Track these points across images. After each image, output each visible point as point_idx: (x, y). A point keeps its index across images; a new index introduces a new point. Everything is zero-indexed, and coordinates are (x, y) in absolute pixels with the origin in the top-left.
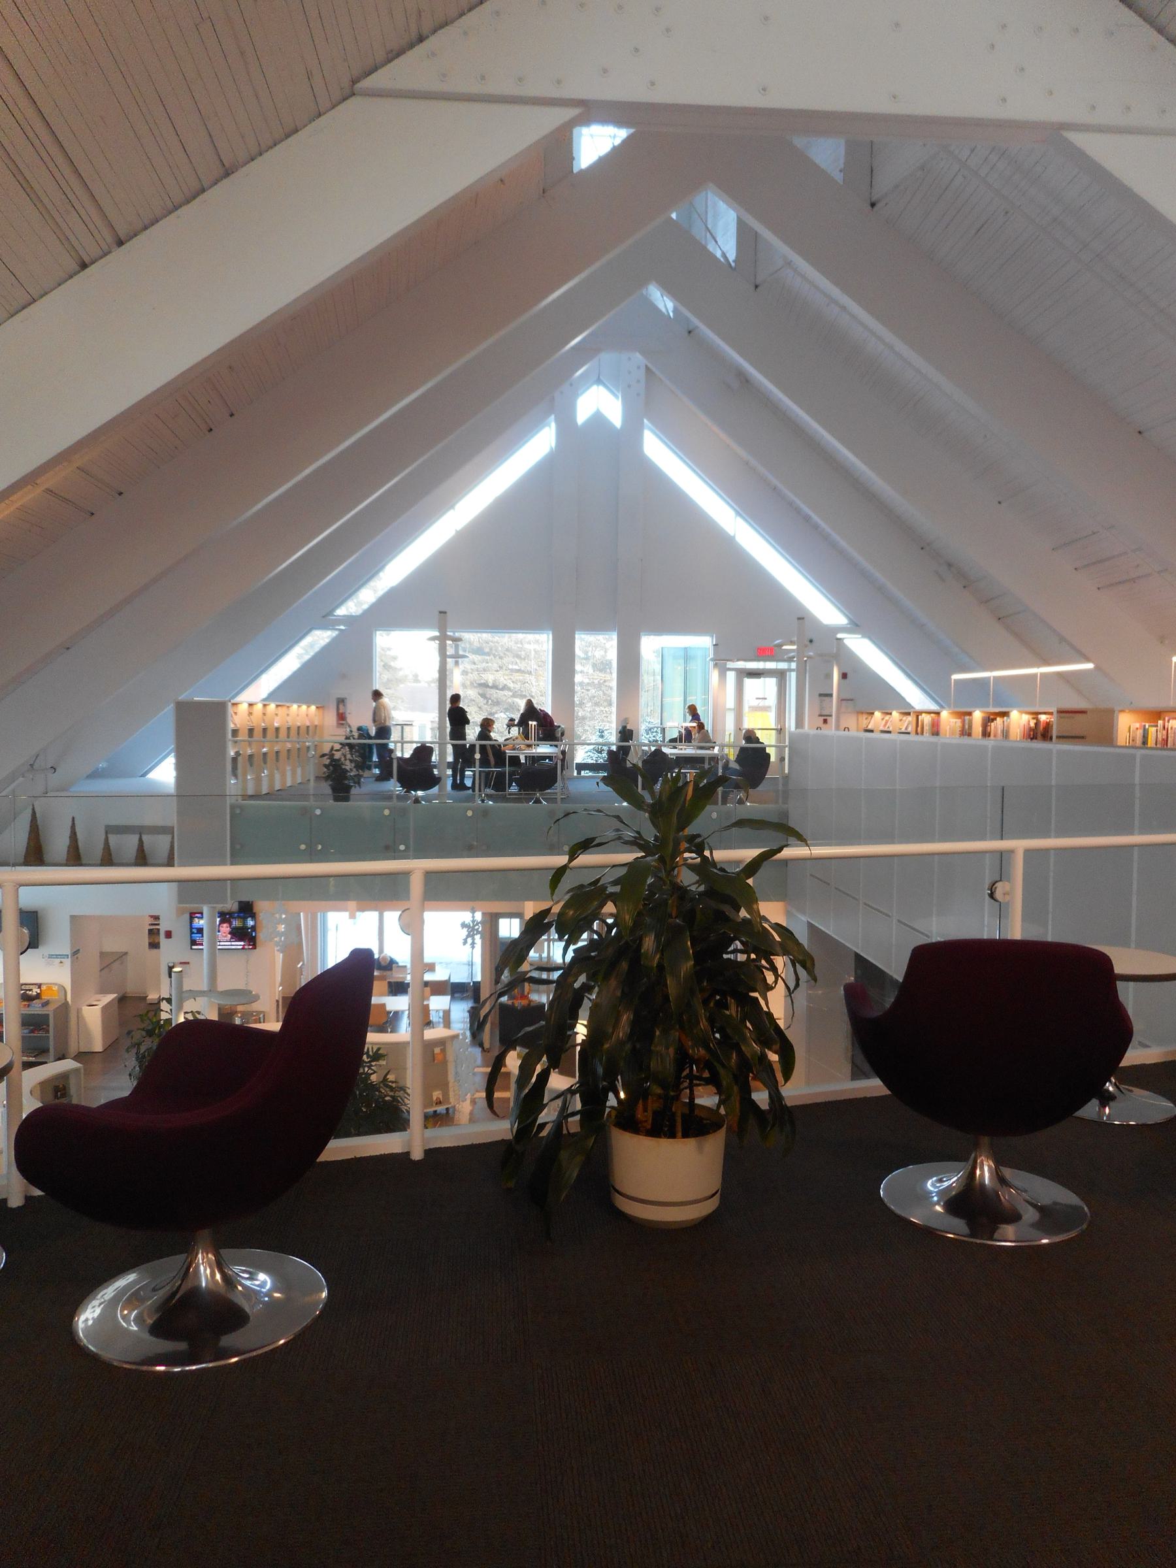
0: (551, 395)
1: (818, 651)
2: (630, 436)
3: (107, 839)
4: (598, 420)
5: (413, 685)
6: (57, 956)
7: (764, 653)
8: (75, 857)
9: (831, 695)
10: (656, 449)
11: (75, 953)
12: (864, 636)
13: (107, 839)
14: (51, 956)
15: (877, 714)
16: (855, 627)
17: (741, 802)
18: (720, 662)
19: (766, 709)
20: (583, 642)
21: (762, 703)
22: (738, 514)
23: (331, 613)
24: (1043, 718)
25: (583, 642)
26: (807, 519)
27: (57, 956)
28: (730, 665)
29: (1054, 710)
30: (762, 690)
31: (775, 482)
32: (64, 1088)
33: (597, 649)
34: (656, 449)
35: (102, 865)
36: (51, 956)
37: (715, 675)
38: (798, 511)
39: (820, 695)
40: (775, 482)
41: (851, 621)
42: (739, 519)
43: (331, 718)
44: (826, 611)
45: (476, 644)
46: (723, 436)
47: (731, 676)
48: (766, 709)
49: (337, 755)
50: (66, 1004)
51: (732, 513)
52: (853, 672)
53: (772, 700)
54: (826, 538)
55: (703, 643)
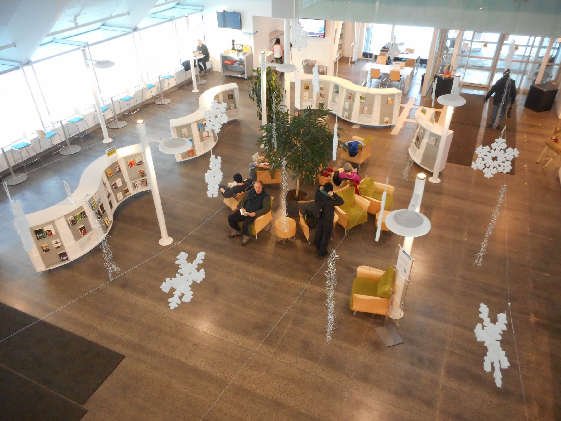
6: (249, 34)
11: (256, 32)
14: (246, 33)
27: (249, 34)
32: (232, 95)
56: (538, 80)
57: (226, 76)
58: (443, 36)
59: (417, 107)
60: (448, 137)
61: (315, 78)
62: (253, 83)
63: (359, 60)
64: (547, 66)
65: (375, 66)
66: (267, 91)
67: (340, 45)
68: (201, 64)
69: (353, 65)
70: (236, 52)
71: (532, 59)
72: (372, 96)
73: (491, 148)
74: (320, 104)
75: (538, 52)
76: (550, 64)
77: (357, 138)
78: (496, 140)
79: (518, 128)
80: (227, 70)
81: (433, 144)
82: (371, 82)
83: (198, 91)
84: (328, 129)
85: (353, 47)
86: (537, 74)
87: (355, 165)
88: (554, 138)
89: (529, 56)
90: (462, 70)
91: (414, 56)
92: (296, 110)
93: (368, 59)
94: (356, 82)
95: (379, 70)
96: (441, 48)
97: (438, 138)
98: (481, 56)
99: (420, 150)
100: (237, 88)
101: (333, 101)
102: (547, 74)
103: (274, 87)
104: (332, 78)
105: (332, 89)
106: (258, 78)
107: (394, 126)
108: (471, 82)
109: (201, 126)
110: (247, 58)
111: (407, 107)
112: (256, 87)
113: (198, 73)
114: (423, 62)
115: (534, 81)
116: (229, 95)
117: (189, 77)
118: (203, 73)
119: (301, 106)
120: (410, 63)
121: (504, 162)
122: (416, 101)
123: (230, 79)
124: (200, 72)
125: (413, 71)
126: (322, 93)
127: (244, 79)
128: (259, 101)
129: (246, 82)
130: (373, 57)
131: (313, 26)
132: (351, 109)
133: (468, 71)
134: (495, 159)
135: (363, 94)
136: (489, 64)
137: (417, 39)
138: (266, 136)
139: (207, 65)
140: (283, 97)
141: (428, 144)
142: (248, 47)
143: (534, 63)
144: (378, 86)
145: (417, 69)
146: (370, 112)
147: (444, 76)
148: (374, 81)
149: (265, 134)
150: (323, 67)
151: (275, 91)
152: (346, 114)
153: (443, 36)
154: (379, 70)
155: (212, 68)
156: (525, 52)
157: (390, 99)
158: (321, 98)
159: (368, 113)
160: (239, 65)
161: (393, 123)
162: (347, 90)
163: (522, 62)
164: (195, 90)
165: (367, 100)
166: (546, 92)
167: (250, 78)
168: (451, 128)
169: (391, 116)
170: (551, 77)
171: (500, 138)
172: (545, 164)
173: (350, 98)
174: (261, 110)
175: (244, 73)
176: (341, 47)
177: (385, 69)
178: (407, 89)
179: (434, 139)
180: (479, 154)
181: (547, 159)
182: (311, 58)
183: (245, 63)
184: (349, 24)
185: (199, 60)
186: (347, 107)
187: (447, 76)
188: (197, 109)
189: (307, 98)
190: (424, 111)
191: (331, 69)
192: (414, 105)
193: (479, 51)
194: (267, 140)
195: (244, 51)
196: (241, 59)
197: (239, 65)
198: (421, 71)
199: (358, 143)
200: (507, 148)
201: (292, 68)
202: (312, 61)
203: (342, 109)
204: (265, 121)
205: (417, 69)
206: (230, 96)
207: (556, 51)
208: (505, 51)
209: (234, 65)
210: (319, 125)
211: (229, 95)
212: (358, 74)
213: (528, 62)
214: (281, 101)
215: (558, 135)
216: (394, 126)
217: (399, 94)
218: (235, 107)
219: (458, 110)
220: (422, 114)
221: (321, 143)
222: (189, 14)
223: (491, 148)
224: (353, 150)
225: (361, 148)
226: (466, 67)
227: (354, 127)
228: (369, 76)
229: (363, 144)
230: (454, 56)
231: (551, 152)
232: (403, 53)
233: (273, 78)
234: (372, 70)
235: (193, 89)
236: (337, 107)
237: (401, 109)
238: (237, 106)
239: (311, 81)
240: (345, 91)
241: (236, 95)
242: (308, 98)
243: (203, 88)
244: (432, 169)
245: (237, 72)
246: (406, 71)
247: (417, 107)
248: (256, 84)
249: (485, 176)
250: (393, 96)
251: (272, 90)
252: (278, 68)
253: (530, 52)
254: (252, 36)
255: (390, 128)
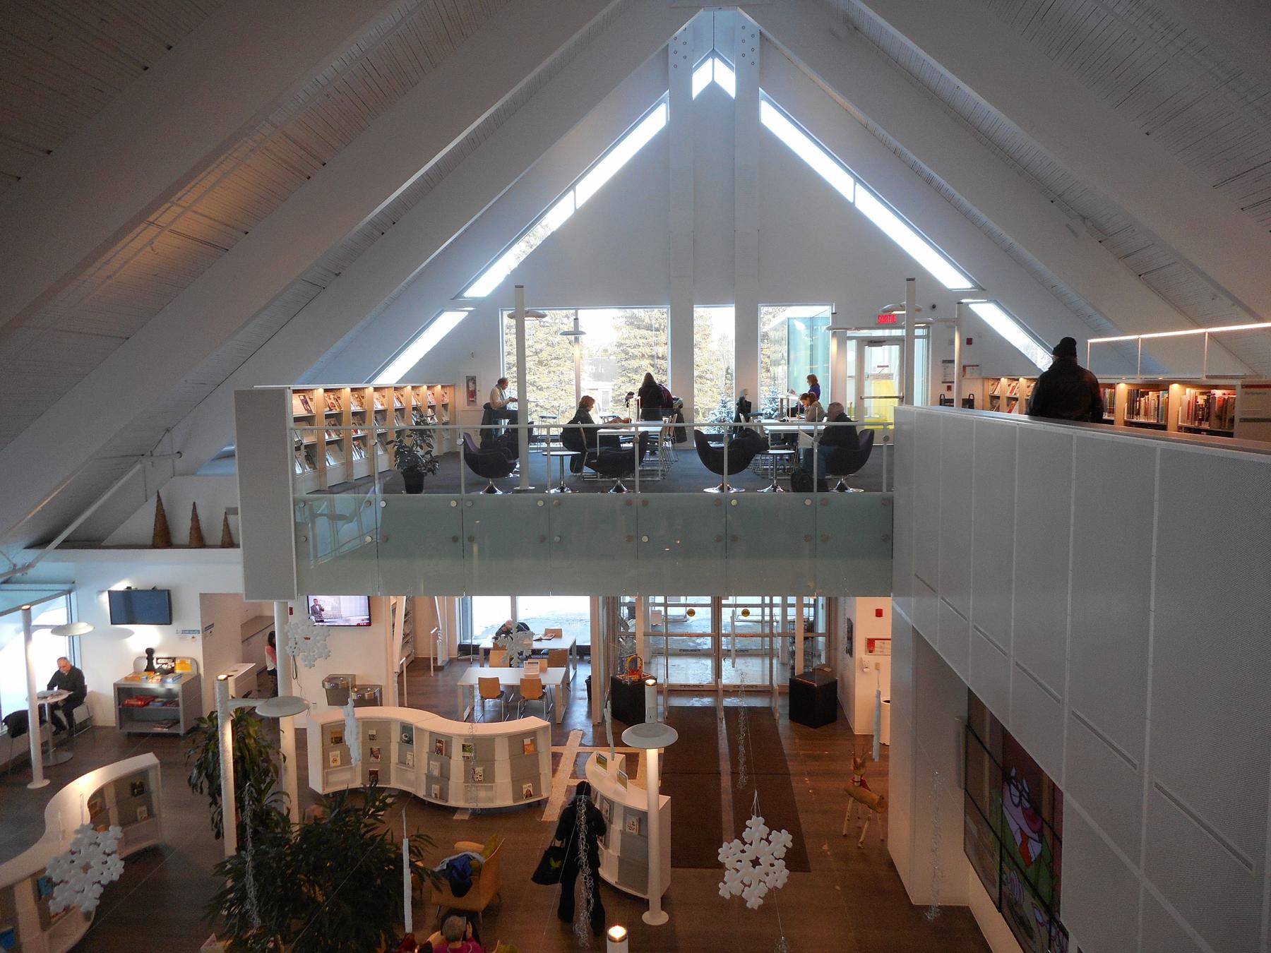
0: (670, 76)
1: (943, 314)
2: (746, 104)
3: (226, 519)
4: (713, 90)
5: (583, 363)
6: (189, 632)
7: (886, 320)
8: (198, 540)
9: (953, 361)
10: (772, 118)
11: (207, 629)
12: (990, 301)
13: (226, 519)
14: (184, 632)
15: (1004, 381)
16: (981, 291)
17: (842, 488)
18: (839, 330)
19: (889, 376)
20: (702, 314)
21: (886, 371)
22: (857, 180)
23: (460, 295)
24: (1218, 393)
25: (702, 314)
26: (929, 181)
27: (189, 632)
28: (849, 333)
29: (1238, 383)
30: (884, 358)
31: (895, 143)
32: (142, 785)
33: (716, 324)
34: (772, 118)
35: (223, 546)
36: (184, 632)
37: (833, 345)
38: (919, 173)
39: (944, 362)
40: (895, 143)
41: (976, 285)
42: (859, 187)
43: (461, 397)
44: (950, 277)
45: (647, 321)
46: (840, 99)
47: (852, 345)
48: (889, 376)
49: (408, 442)
50: (199, 676)
51: (851, 180)
52: (978, 336)
53: (895, 368)
54: (949, 200)
55: (823, 312)
56: (800, 668)
57: (129, 734)
58: (612, 605)
59: (588, 749)
60: (661, 812)
61: (351, 716)
62: (199, 750)
63: (451, 661)
64: (806, 639)
65: (487, 672)
66: (235, 763)
67: (405, 635)
68: (60, 714)
69: (440, 674)
70: (158, 677)
71: (778, 628)
72: (490, 740)
73: (744, 843)
74: (371, 773)
75: (784, 614)
76: (809, 635)
77: (468, 847)
78: (748, 823)
79: (792, 767)
80: (132, 720)
81: (635, 832)
82: (483, 707)
83: (47, 782)
84: (392, 844)
85: (436, 636)
86: (793, 654)
87: (471, 916)
88: (857, 778)
89: (771, 621)
90: (662, 660)
91: (564, 644)
92: (316, 797)
93: (471, 657)
94: (451, 714)
95: (497, 679)
96: (610, 622)
97: (642, 817)
98: (690, 631)
99: (610, 851)
100: (154, 767)
101: (402, 762)
102: (810, 654)
103: (255, 752)
104: (393, 712)
105: (396, 735)
106: (213, 738)
107: (546, 801)
108: (683, 682)
109: (43, 885)
110: (185, 687)
111: (569, 751)
112: (206, 758)
113: (49, 737)
114: (582, 653)
115: (793, 668)
116: (133, 787)
117: (22, 750)
118: (63, 735)
119: (326, 783)
120: (557, 658)
121: (772, 865)
122: (584, 734)
123: (134, 743)
124: (55, 734)
125: (567, 673)
126: (375, 748)
127: (177, 736)
128: (216, 792)
129: (182, 742)
130: (482, 653)
131: (345, 608)
132: (445, 776)
133: (673, 661)
134: (756, 862)
135: (467, 738)
136: (707, 643)
137: (564, 615)
138: (231, 890)
139: (75, 716)
140: (277, 772)
141: (623, 833)
142: (188, 662)
143: (783, 635)
144: (498, 718)
145: (575, 668)
146: (489, 777)
147: (627, 679)
148: (489, 703)
149: (229, 884)
150: (373, 687)
151: (257, 764)
152: (435, 788)
153: (612, 605)
154: (497, 679)
155: (90, 719)
156: (763, 615)
157: (527, 741)
158: (373, 759)
159: (485, 781)
160: (165, 704)
161: (545, 795)
162: (431, 733)
163: (763, 636)
164: (39, 783)
165: (478, 749)
166: (820, 688)
167: (193, 730)
168: (662, 791)
169: (536, 780)
170: (820, 656)
171: (754, 817)
172: (859, 838)
173: (439, 751)
174: (221, 813)
175: (178, 722)
176: (408, 639)
177: (508, 676)
178: (561, 711)
179: (635, 820)
180: (726, 861)
181: (860, 823)
182: (341, 669)
183: (180, 699)
184: (422, 601)
185: (54, 707)
186: (436, 773)
187: (635, 678)
188: (35, 840)
189: (339, 763)
190: (602, 761)
191: (391, 692)
192: (581, 745)
193: (679, 621)
194: (236, 898)
195: (178, 671)
196: (169, 690)
197: (165, 704)
198: (583, 673)
199: (469, 858)
200: (770, 834)
201: (298, 705)
202: (345, 677)
203: (424, 778)
204: (230, 844)
205: (575, 668)
206: (135, 787)
207: (812, 610)
208: (726, 614)
209: (151, 706)
210: (368, 836)
211: (133, 787)
212: (453, 692)
213: (771, 635)
214: (272, 781)
215: (862, 771)
216: (546, 801)
217: (545, 728)
218: (150, 814)
219: (665, 759)
220: (599, 768)
221: (379, 882)
222: (32, 604)
223: (744, 843)
224: (461, 877)
225: (479, 870)
226: (668, 654)
227: (456, 817)
228: (477, 693)
229: (482, 859)
230: (640, 635)
231: (861, 807)
232: (540, 640)
233: (251, 731)
234: (482, 681)
235: (30, 778)
236: (409, 776)
237: (556, 758)
238: (155, 811)
239: (342, 725)
240: (427, 736)
241: (154, 783)
242: (342, 764)
243: (62, 775)
244: (646, 892)
245: (159, 723)
246: (553, 677)
247: (588, 749)
248: (206, 750)
249: (748, 905)
250: (532, 733)
251: (248, 761)
252: (263, 709)
253: (771, 615)
254: (199, 637)
255: (540, 805)
